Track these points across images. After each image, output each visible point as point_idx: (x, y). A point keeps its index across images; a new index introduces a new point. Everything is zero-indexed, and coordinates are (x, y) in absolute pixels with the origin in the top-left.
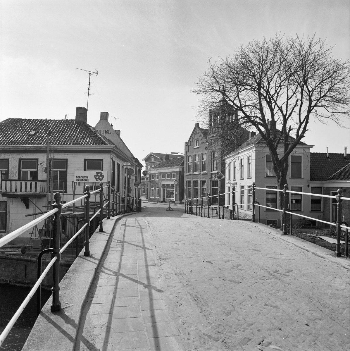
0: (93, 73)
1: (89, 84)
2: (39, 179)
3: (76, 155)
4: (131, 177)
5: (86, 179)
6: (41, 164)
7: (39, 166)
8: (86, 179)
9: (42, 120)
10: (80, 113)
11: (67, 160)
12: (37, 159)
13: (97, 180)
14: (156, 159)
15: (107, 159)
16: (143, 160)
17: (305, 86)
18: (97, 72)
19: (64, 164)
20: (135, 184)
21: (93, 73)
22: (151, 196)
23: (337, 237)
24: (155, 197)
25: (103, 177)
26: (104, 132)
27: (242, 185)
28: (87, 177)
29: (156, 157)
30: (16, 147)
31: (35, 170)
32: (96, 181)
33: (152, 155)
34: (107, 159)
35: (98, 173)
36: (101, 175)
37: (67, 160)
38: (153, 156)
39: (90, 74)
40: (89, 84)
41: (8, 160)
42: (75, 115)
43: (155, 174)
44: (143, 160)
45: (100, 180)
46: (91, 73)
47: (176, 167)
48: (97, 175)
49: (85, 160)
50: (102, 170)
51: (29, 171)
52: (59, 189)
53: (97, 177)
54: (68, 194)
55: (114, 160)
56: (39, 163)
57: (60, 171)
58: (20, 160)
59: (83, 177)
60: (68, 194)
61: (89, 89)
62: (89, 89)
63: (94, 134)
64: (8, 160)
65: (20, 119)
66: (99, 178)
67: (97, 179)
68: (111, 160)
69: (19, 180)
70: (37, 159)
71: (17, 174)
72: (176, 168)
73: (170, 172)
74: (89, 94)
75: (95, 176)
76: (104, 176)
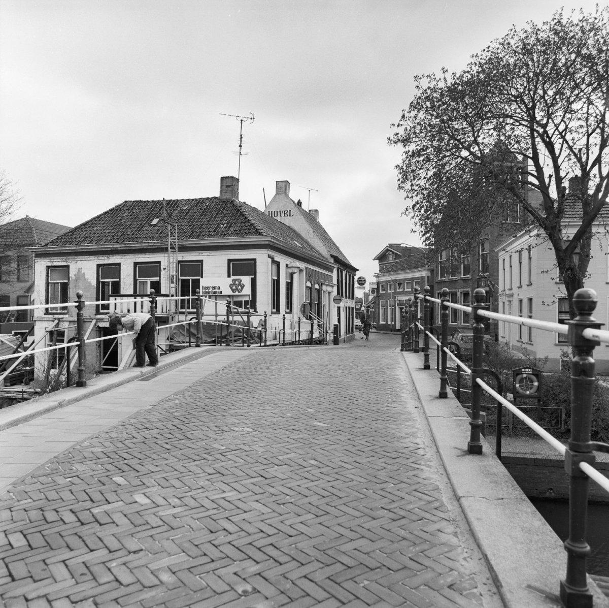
0: (246, 119)
1: (241, 138)
2: (122, 293)
3: (213, 254)
4: (324, 288)
5: (218, 290)
6: (165, 269)
7: (163, 273)
8: (218, 290)
9: (170, 201)
10: (227, 187)
11: (202, 261)
12: (159, 263)
13: (234, 292)
14: (397, 256)
15: (262, 258)
16: (374, 260)
17: (564, 79)
18: (252, 116)
19: (197, 268)
20: (334, 300)
21: (246, 119)
22: (381, 320)
23: (591, 417)
24: (387, 322)
25: (243, 287)
26: (283, 215)
27: (520, 297)
28: (219, 288)
29: (396, 254)
30: (129, 245)
31: (156, 279)
32: (231, 293)
33: (389, 250)
34: (262, 258)
35: (234, 280)
36: (240, 284)
37: (202, 261)
38: (391, 251)
39: (242, 120)
40: (241, 138)
41: (119, 264)
42: (219, 189)
43: (387, 282)
44: (374, 260)
45: (239, 292)
46: (243, 119)
47: (419, 269)
48: (234, 284)
49: (229, 261)
50: (202, 277)
51: (149, 280)
52: (192, 308)
53: (234, 288)
54: (258, 313)
55: (276, 259)
56: (162, 269)
57: (192, 279)
58: (136, 264)
59: (212, 287)
60: (258, 313)
61: (240, 146)
62: (240, 146)
63: (246, 218)
64: (119, 264)
65: (141, 201)
66: (237, 289)
67: (233, 291)
68: (270, 260)
69: (135, 295)
70: (159, 263)
71: (132, 286)
72: (421, 271)
73: (410, 279)
74: (240, 154)
75: (231, 285)
76: (244, 286)
